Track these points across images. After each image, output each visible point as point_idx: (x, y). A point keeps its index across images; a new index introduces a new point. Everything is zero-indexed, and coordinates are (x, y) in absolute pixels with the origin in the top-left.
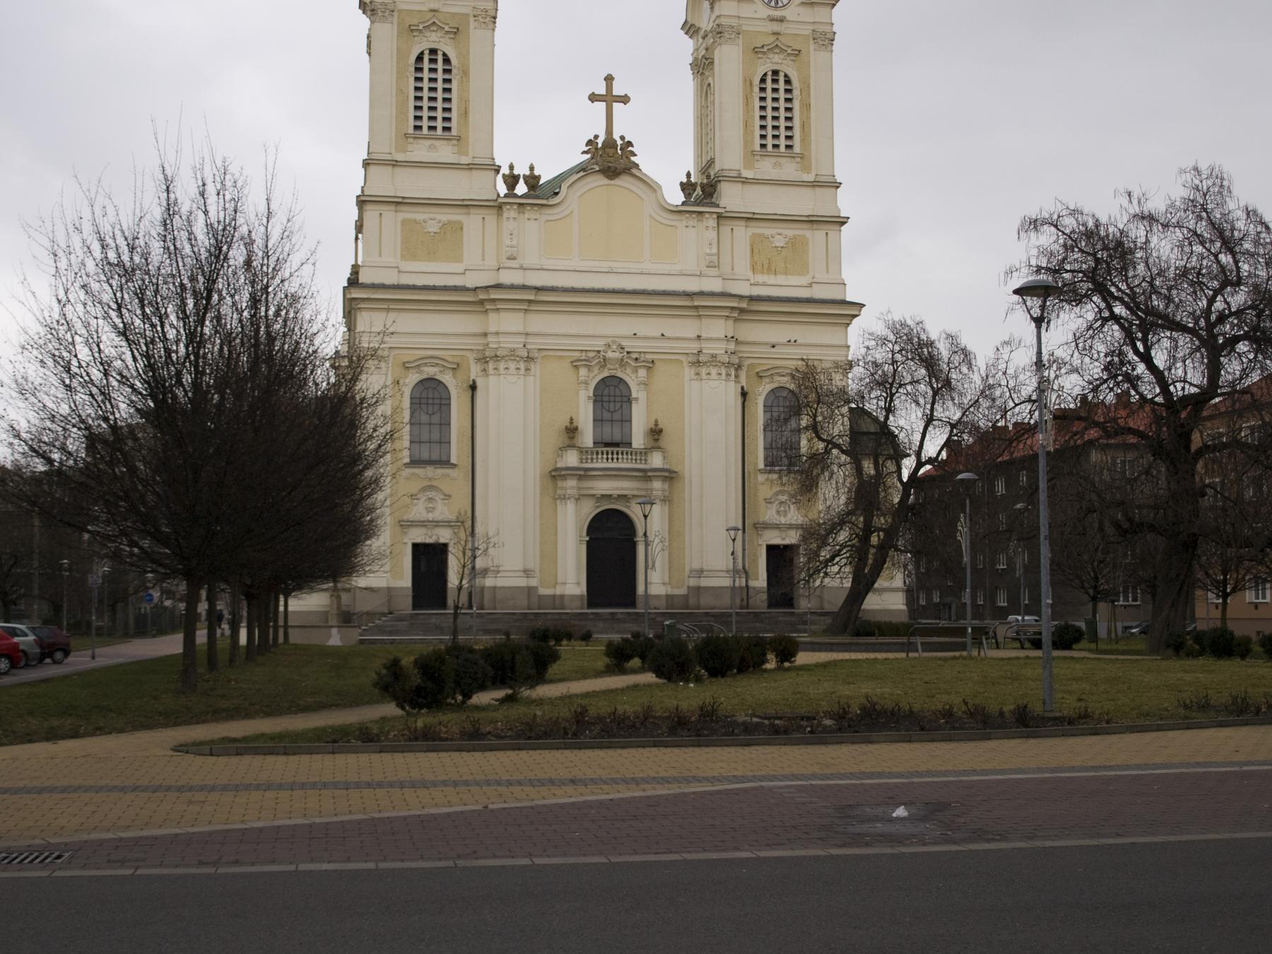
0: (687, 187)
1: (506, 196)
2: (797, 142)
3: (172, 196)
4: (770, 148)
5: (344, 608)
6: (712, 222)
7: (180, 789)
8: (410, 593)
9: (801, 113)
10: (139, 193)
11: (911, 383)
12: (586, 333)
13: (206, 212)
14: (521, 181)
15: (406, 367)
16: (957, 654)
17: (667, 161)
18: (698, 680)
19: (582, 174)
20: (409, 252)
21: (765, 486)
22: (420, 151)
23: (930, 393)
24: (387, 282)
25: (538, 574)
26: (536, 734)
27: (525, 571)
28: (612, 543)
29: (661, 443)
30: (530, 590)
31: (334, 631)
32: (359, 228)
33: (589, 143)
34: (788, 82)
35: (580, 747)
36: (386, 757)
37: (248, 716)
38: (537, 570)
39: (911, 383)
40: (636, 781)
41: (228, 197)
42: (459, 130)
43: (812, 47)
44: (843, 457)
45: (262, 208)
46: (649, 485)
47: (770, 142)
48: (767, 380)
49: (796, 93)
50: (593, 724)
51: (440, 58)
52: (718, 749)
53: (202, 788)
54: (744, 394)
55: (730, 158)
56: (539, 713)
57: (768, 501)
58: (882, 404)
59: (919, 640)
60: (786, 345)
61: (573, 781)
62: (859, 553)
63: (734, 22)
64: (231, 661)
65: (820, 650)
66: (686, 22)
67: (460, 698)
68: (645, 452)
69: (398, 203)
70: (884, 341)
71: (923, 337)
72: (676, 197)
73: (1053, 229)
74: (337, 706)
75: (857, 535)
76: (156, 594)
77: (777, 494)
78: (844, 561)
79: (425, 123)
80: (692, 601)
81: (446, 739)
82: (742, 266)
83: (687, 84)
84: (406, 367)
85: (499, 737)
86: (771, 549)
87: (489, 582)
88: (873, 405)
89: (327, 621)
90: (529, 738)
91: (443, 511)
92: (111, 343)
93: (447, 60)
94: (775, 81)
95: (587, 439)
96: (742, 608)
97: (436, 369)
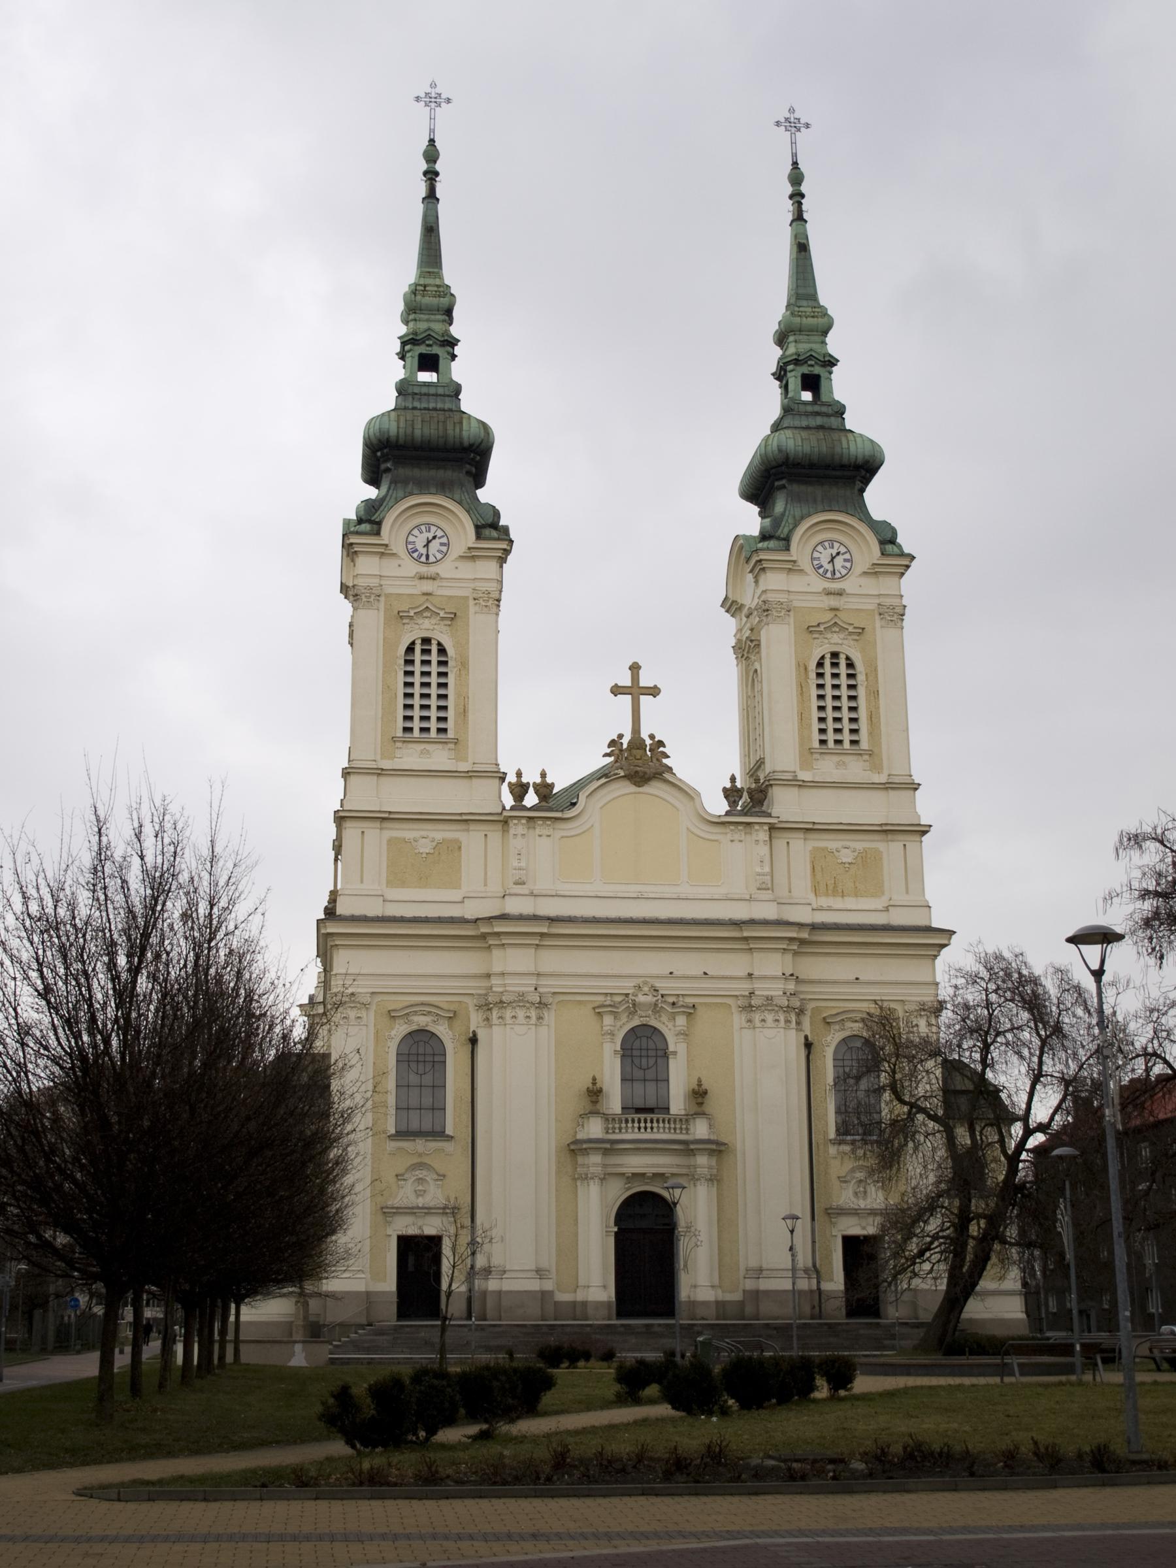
0: (731, 794)
1: (512, 808)
2: (864, 736)
3: (104, 839)
4: (831, 744)
5: (312, 1318)
6: (763, 835)
7: (77, 1540)
8: (395, 1299)
10: (66, 839)
11: (1011, 1030)
12: (610, 972)
13: (142, 857)
14: (531, 790)
15: (392, 1016)
16: (1063, 1378)
17: (707, 761)
18: (725, 1412)
19: (603, 780)
20: (396, 878)
21: (839, 1163)
22: (410, 757)
23: (1037, 1042)
24: (370, 914)
25: (553, 1275)
26: (500, 1480)
27: (538, 1271)
28: (646, 1236)
29: (707, 1108)
30: (544, 1295)
31: (298, 1348)
32: (338, 848)
33: (612, 743)
34: (850, 665)
35: (553, 1495)
36: (323, 1505)
37: (170, 1454)
38: (554, 1270)
39: (1011, 1030)
40: (609, 1536)
41: (167, 841)
43: (878, 624)
44: (931, 1124)
45: (206, 852)
46: (691, 1161)
47: (831, 736)
48: (837, 1027)
49: (861, 678)
50: (575, 1467)
51: (434, 648)
52: (719, 1499)
53: (103, 1539)
54: (808, 1045)
55: (783, 757)
56: (506, 1453)
57: (843, 1180)
58: (977, 1056)
59: (1015, 1361)
60: (858, 983)
61: (534, 1536)
62: (956, 1245)
63: (783, 598)
64: (161, 1386)
65: (895, 1374)
66: (726, 598)
67: (422, 1434)
68: (686, 1120)
69: (384, 819)
70: (974, 979)
71: (1025, 972)
72: (718, 806)
73: (1158, 844)
74: (278, 1442)
75: (953, 1225)
76: (83, 1299)
77: (853, 1170)
78: (937, 1256)
79: (416, 724)
80: (749, 1309)
81: (395, 1485)
82: (802, 887)
83: (729, 670)
84: (392, 1016)
85: (459, 1482)
86: (850, 1243)
87: (493, 1285)
88: (971, 1056)
89: (291, 1335)
90: (495, 1483)
91: (434, 1196)
92: (32, 1010)
93: (442, 651)
94: (835, 665)
95: (614, 1103)
96: (812, 1318)
97: (428, 1019)
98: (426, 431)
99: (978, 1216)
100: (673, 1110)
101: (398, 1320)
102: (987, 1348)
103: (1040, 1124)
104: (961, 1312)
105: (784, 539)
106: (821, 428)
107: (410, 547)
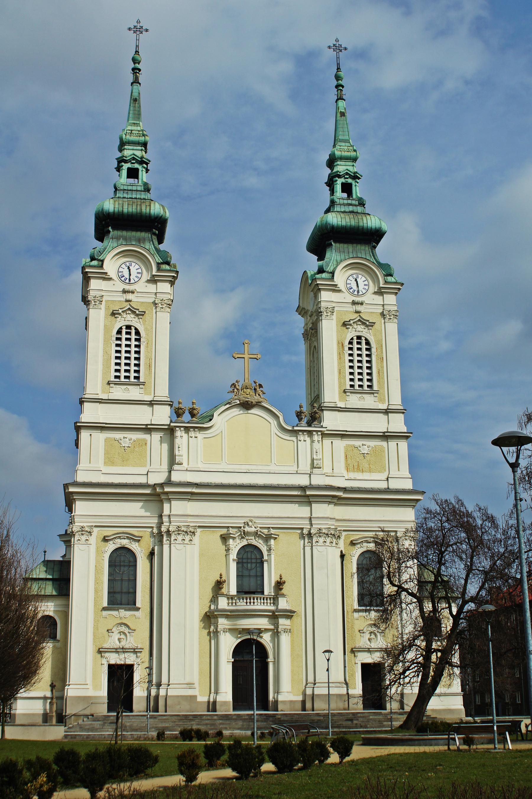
8: (106, 701)
9: (377, 363)
19: (228, 406)
20: (109, 461)
28: (252, 663)
33: (233, 385)
42: (145, 378)
49: (374, 350)
54: (342, 556)
71: (463, 509)
75: (422, 655)
78: (413, 674)
82: (340, 467)
86: (365, 667)
93: (137, 333)
96: (345, 709)
98: (130, 210)
99: (436, 651)
100: (266, 592)
101: (108, 712)
102: (443, 728)
103: (472, 597)
104: (427, 705)
105: (331, 273)
106: (352, 212)
107: (120, 274)
